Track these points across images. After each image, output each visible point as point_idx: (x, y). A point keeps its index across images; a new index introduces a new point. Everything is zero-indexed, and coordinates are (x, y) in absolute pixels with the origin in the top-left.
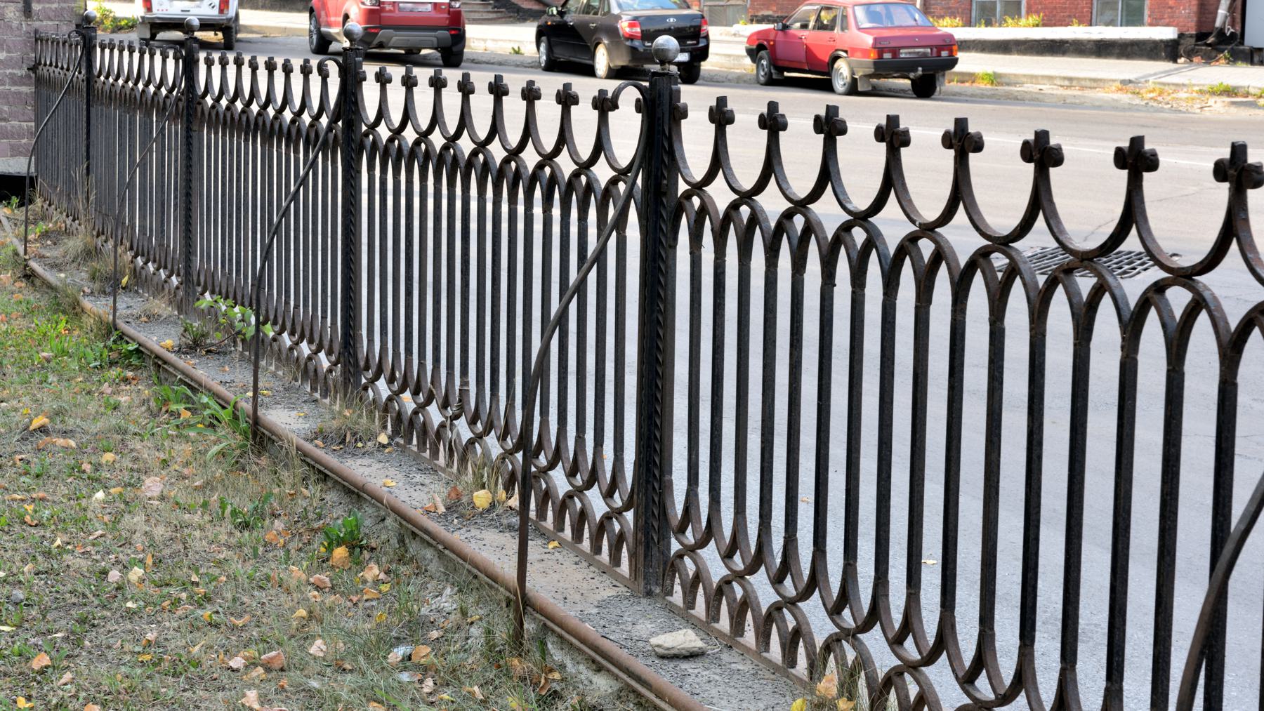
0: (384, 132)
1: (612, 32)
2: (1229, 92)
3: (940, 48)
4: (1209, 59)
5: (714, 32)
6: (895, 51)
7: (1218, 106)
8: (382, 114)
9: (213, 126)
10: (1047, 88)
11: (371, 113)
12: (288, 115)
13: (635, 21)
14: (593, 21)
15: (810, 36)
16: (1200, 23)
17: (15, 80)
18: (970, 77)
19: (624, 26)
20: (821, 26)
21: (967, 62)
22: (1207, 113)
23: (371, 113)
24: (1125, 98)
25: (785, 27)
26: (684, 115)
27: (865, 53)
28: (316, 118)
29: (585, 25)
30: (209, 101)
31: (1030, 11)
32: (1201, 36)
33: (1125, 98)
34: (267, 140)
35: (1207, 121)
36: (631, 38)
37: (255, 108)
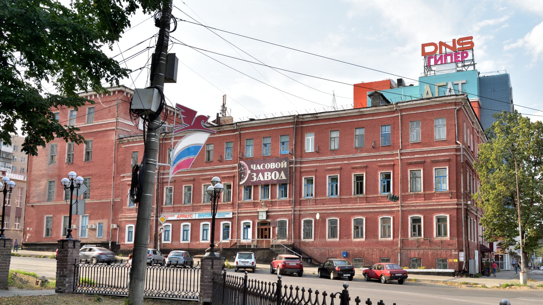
0: (286, 299)
1: (334, 270)
2: (466, 284)
3: (404, 274)
4: (462, 276)
5: (356, 269)
6: (394, 274)
7: (464, 286)
8: (285, 294)
9: (249, 295)
10: (427, 282)
11: (283, 295)
12: (265, 293)
13: (339, 267)
14: (330, 267)
15: (376, 271)
16: (459, 269)
17: (209, 282)
18: (411, 280)
19: (337, 268)
20: (378, 269)
21: (410, 277)
22: (462, 288)
23: (283, 295)
24: (444, 285)
25: (371, 269)
26: (350, 300)
27: (388, 274)
28: (271, 295)
29: (328, 268)
30: (249, 289)
31: (423, 266)
32: (460, 271)
33: (444, 285)
34: (261, 299)
35: (462, 290)
36: (338, 271)
37: (258, 291)
